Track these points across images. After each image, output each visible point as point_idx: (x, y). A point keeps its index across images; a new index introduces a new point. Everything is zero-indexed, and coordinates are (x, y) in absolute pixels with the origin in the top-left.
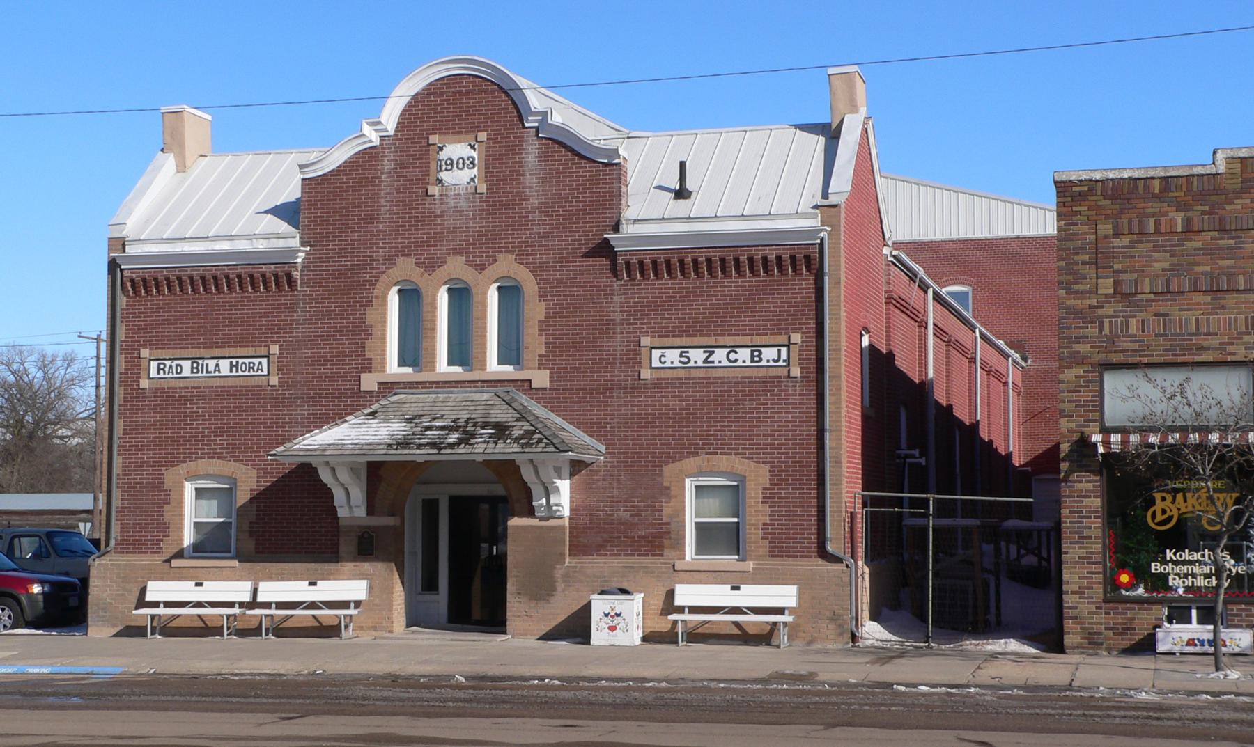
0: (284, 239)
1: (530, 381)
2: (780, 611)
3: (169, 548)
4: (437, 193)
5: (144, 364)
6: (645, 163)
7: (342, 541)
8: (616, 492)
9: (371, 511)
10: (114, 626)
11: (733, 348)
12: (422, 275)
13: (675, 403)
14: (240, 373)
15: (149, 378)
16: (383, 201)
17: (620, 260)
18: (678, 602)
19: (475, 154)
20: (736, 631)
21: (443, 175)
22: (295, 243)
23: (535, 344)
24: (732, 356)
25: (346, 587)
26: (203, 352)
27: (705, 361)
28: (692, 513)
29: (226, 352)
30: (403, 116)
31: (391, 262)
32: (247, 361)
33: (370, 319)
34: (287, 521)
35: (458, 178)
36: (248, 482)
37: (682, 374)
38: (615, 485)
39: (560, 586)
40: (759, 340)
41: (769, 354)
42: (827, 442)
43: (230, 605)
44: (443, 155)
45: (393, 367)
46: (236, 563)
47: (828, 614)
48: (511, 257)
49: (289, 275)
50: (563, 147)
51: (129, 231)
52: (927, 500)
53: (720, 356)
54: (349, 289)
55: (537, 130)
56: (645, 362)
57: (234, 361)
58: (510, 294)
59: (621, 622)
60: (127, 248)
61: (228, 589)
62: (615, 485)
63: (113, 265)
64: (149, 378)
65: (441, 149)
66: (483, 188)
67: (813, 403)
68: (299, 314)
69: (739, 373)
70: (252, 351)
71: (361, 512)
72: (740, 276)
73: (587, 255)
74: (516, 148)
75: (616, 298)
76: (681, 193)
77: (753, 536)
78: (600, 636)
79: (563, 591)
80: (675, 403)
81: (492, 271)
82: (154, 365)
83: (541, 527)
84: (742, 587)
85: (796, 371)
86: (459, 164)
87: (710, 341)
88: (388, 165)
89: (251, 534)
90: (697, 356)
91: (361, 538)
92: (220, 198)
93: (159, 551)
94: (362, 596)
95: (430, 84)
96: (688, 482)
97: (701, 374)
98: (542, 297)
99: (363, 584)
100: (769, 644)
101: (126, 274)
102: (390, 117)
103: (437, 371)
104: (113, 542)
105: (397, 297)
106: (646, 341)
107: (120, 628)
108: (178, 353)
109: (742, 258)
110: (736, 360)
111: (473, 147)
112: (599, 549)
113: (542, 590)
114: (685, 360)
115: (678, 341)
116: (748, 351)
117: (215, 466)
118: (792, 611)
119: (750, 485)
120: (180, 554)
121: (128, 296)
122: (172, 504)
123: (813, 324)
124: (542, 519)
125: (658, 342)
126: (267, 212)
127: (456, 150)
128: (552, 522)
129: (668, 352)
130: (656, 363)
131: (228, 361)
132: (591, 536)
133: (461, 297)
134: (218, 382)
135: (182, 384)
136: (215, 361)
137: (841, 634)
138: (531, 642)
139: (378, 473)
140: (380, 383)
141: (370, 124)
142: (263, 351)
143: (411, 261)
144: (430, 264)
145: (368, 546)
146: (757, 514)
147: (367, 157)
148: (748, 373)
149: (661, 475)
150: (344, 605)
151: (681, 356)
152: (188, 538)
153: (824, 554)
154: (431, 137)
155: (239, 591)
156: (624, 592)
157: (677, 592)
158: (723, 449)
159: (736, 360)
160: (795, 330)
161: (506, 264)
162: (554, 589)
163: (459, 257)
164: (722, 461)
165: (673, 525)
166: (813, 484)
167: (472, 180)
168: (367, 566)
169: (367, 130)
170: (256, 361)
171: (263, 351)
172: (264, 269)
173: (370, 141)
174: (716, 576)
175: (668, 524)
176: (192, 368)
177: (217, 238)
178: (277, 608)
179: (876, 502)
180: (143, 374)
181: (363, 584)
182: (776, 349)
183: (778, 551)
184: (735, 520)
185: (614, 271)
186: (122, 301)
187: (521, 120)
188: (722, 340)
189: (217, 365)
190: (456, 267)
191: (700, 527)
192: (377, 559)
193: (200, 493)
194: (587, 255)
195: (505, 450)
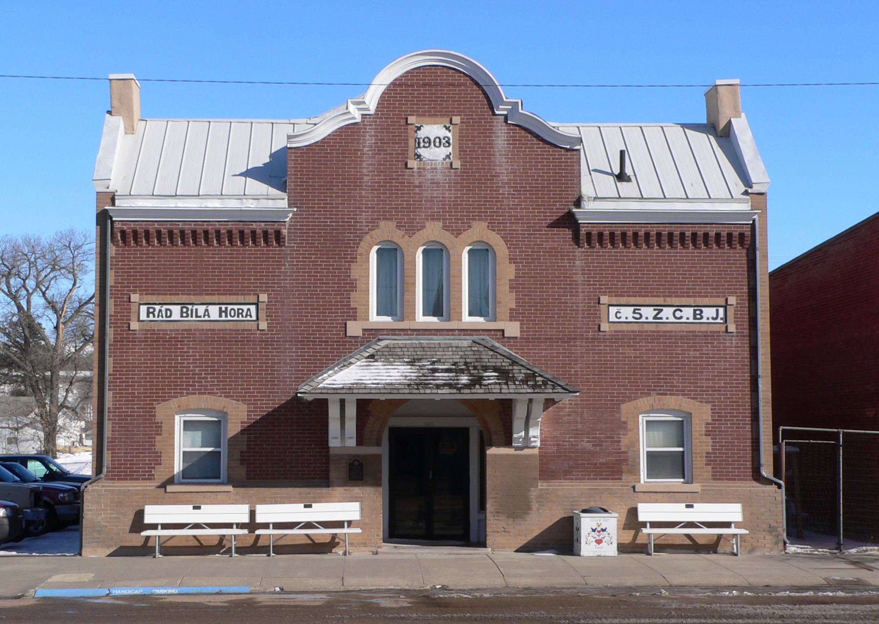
0: (268, 200)
1: (503, 331)
2: (727, 525)
3: (161, 475)
4: (416, 167)
5: (134, 308)
6: (597, 148)
7: (332, 467)
8: (580, 426)
9: (360, 441)
10: (108, 547)
11: (659, 308)
12: (403, 237)
13: (630, 352)
14: (229, 318)
15: (139, 321)
16: (365, 171)
17: (583, 231)
18: (148, 520)
19: (450, 135)
20: (688, 542)
21: (420, 151)
22: (283, 204)
23: (507, 300)
24: (678, 314)
25: (343, 509)
26: (193, 298)
27: (655, 317)
28: (646, 442)
29: (216, 298)
30: (382, 97)
31: (374, 224)
32: (236, 307)
33: (355, 273)
34: (282, 447)
35: (436, 155)
36: (238, 416)
37: (636, 328)
38: (579, 420)
39: (535, 506)
40: (700, 301)
41: (709, 313)
42: (760, 386)
43: (229, 526)
44: (421, 134)
45: (375, 318)
46: (230, 488)
47: (765, 527)
48: (484, 224)
49: (278, 234)
50: (532, 135)
51: (114, 186)
52: (839, 433)
53: (667, 313)
54: (336, 247)
55: (506, 117)
56: (603, 316)
57: (223, 307)
58: (481, 255)
59: (599, 537)
60: (117, 202)
61: (226, 512)
62: (579, 420)
63: (103, 218)
64: (139, 321)
65: (419, 128)
66: (457, 164)
67: (747, 354)
68: (286, 267)
69: (684, 328)
70: (241, 299)
71: (352, 442)
72: (268, 246)
73: (552, 225)
74: (488, 132)
75: (577, 263)
76: (621, 177)
77: (698, 464)
78: (588, 548)
79: (538, 509)
80: (630, 352)
81: (466, 236)
82: (143, 309)
83: (518, 455)
84: (313, 505)
85: (732, 328)
86: (436, 143)
87: (660, 301)
88: (369, 140)
89: (242, 461)
90: (648, 313)
91: (351, 465)
92: (198, 162)
93: (151, 478)
94: (356, 516)
95: (407, 72)
96: (177, 418)
97: (652, 328)
98: (512, 260)
99: (356, 506)
100: (715, 552)
101: (117, 225)
102: (372, 98)
103: (370, 320)
104: (105, 470)
105: (375, 255)
106: (604, 299)
107: (115, 549)
108: (168, 299)
109: (687, 234)
110: (681, 318)
111: (447, 128)
112: (566, 474)
113: (518, 508)
114: (638, 316)
115: (632, 300)
116: (692, 309)
117: (207, 401)
118: (738, 525)
119: (695, 421)
120: (171, 481)
121: (117, 246)
122: (164, 435)
123: (745, 289)
124: (517, 448)
125: (614, 300)
126: (241, 175)
127: (433, 130)
128: (526, 451)
129: (623, 309)
130: (612, 318)
131: (217, 307)
132: (553, 465)
133: (435, 255)
134: (206, 326)
135: (172, 326)
136: (204, 307)
137: (777, 543)
138: (510, 554)
139: (369, 408)
140: (364, 330)
141: (355, 103)
142: (253, 299)
143: (392, 225)
144: (411, 228)
145: (357, 473)
146: (701, 444)
147: (349, 133)
148: (692, 328)
149: (619, 412)
150: (339, 524)
151: (634, 312)
152: (178, 466)
153: (757, 476)
154: (454, 118)
155: (238, 513)
156: (605, 511)
157: (639, 510)
158: (671, 391)
159: (681, 318)
160: (731, 294)
161: (480, 231)
162: (531, 509)
163: (436, 223)
164: (672, 401)
165: (630, 454)
166: (748, 420)
167: (448, 156)
168: (357, 491)
169: (352, 108)
170: (245, 308)
171: (253, 299)
172: (254, 226)
173: (354, 118)
174: (670, 496)
175: (626, 453)
176: (182, 312)
177: (208, 196)
178: (274, 528)
179: (787, 434)
180: (133, 317)
181: (356, 506)
182: (714, 309)
183: (717, 476)
184: (681, 449)
185: (576, 239)
186: (111, 250)
187: (492, 108)
188: (669, 301)
189: (207, 310)
190: (434, 231)
191: (650, 455)
192: (366, 484)
193: (188, 425)
194: (552, 225)
195: (508, 391)
